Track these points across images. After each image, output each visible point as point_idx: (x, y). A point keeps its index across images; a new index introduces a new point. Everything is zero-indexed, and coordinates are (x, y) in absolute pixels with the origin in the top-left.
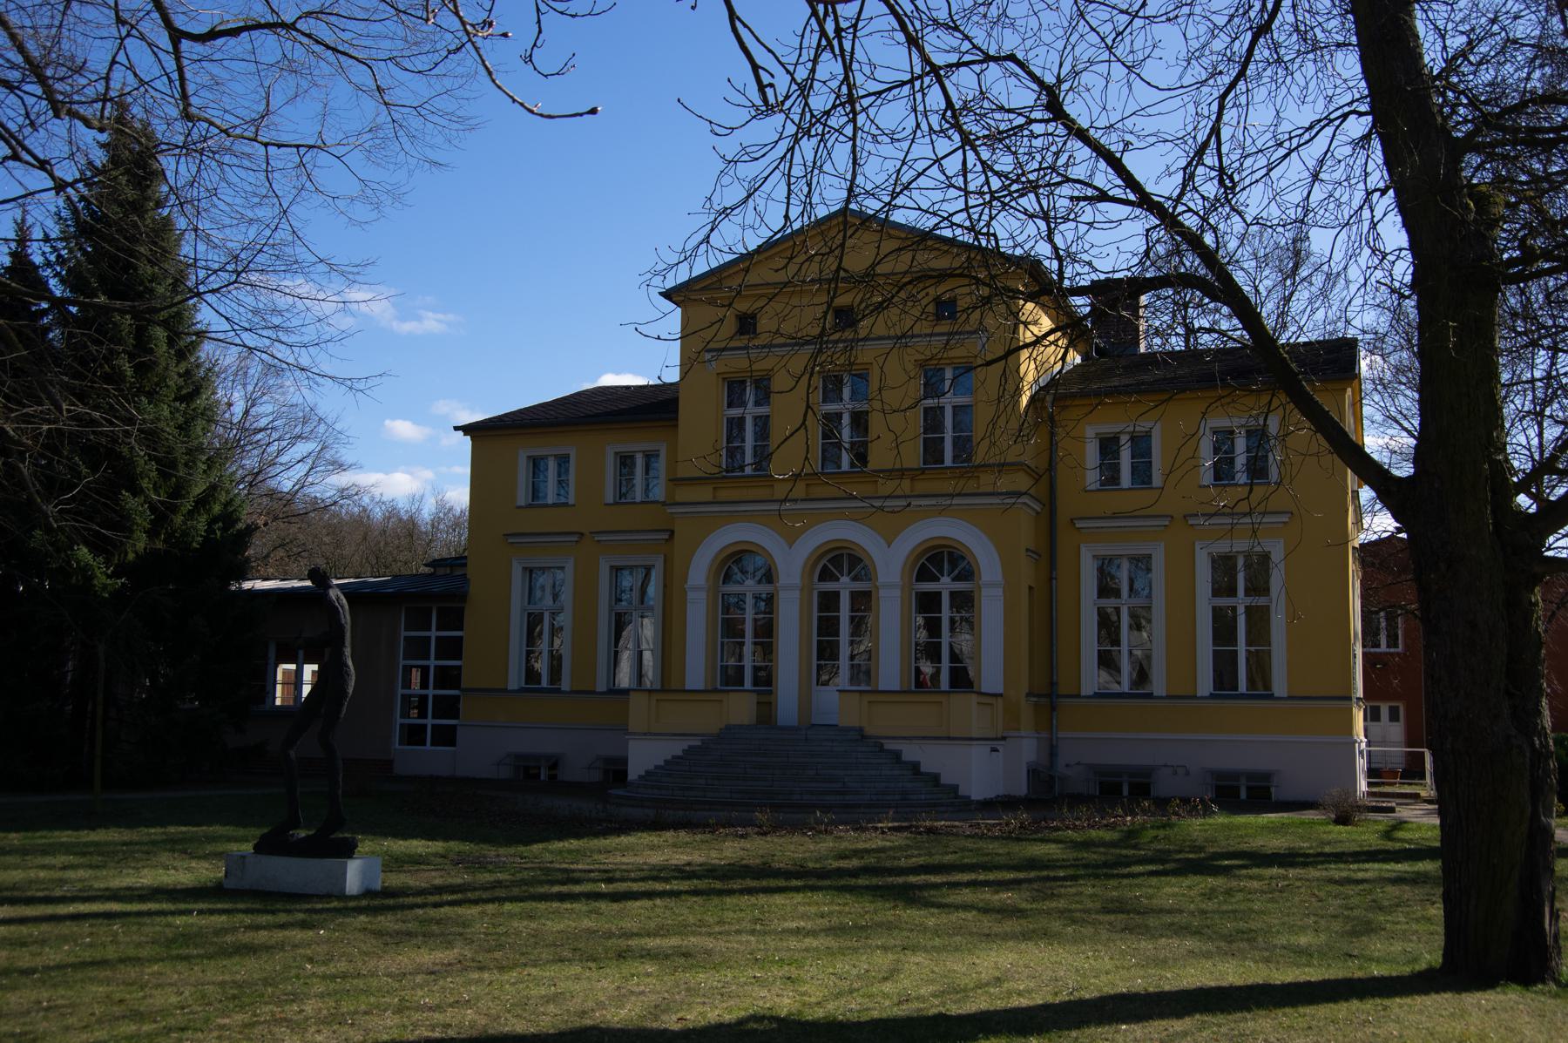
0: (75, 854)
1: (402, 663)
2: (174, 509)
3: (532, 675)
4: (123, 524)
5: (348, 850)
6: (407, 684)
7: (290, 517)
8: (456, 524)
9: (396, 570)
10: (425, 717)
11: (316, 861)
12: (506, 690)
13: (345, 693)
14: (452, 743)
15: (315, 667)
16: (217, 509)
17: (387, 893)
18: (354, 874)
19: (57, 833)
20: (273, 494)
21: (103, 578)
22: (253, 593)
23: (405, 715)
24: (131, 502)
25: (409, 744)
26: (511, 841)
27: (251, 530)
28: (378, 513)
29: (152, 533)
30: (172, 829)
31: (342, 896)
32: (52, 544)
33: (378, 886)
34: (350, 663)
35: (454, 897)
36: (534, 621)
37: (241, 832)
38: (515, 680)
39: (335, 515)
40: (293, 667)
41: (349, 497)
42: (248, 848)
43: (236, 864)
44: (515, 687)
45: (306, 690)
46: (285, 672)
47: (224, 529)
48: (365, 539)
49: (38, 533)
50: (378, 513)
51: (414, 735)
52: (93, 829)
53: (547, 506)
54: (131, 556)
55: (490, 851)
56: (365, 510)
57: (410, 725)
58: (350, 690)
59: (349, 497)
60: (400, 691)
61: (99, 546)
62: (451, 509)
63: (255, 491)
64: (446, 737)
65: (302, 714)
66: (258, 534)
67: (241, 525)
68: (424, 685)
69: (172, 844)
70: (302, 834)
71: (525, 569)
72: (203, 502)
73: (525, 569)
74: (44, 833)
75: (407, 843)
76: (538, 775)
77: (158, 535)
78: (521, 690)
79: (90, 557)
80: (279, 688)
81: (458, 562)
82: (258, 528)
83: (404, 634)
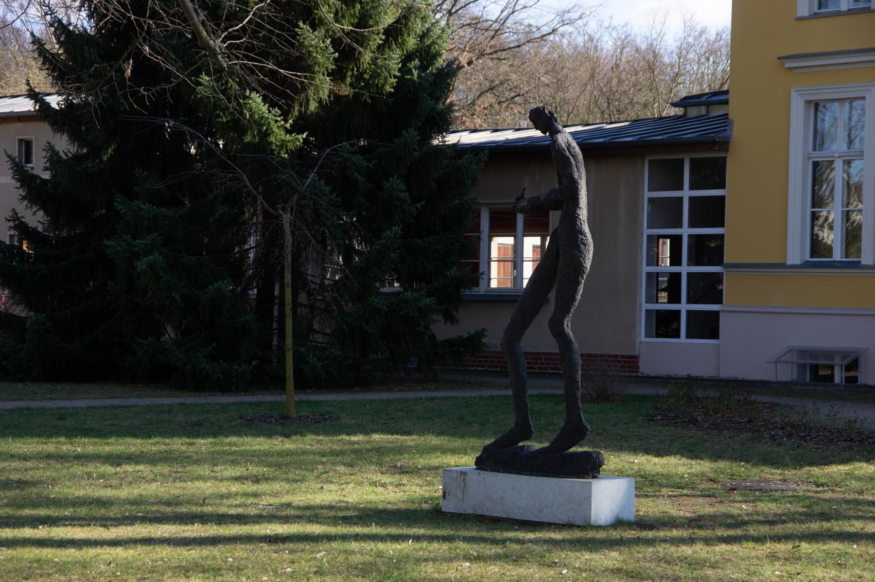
0: (270, 465)
1: (646, 231)
2: (362, 40)
3: (817, 247)
4: (301, 62)
5: (590, 467)
6: (654, 259)
7: (498, 52)
8: (711, 51)
9: (633, 116)
10: (678, 301)
11: (553, 481)
12: (783, 265)
13: (580, 268)
14: (714, 334)
15: (537, 240)
16: (411, 42)
17: (642, 524)
18: (607, 496)
19: (248, 439)
20: (475, 23)
21: (282, 135)
22: (459, 150)
23: (652, 298)
24: (312, 38)
25: (658, 336)
26: (799, 462)
27: (451, 71)
28: (608, 44)
29: (337, 75)
30: (376, 437)
31: (587, 526)
32: (223, 92)
33: (630, 516)
34: (586, 228)
35: (732, 533)
36: (819, 172)
37: (458, 443)
38: (797, 252)
39: (555, 47)
40: (510, 240)
41: (571, 22)
42: (468, 461)
43: (455, 480)
44: (798, 262)
45: (528, 270)
46: (501, 248)
47: (422, 68)
48: (592, 76)
49: (205, 78)
50: (608, 44)
51: (665, 325)
52: (287, 436)
53: (839, 14)
54: (313, 106)
55: (771, 474)
56: (591, 39)
57: (658, 312)
58: (588, 264)
59: (571, 22)
60: (645, 269)
61: (280, 94)
62: (702, 32)
63: (455, 21)
64: (706, 327)
65: (523, 304)
66: (461, 75)
67: (440, 62)
68: (676, 259)
69: (378, 456)
70: (536, 445)
71: (808, 102)
72: (394, 33)
73: (808, 102)
74: (234, 439)
75: (664, 460)
76: (831, 378)
77: (343, 78)
78: (806, 265)
79: (264, 108)
80: (494, 266)
81: (716, 98)
82: (460, 67)
83: (647, 194)
